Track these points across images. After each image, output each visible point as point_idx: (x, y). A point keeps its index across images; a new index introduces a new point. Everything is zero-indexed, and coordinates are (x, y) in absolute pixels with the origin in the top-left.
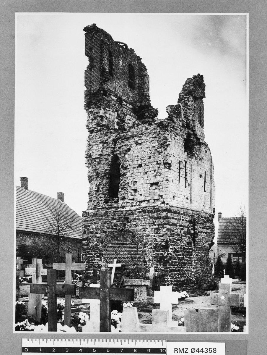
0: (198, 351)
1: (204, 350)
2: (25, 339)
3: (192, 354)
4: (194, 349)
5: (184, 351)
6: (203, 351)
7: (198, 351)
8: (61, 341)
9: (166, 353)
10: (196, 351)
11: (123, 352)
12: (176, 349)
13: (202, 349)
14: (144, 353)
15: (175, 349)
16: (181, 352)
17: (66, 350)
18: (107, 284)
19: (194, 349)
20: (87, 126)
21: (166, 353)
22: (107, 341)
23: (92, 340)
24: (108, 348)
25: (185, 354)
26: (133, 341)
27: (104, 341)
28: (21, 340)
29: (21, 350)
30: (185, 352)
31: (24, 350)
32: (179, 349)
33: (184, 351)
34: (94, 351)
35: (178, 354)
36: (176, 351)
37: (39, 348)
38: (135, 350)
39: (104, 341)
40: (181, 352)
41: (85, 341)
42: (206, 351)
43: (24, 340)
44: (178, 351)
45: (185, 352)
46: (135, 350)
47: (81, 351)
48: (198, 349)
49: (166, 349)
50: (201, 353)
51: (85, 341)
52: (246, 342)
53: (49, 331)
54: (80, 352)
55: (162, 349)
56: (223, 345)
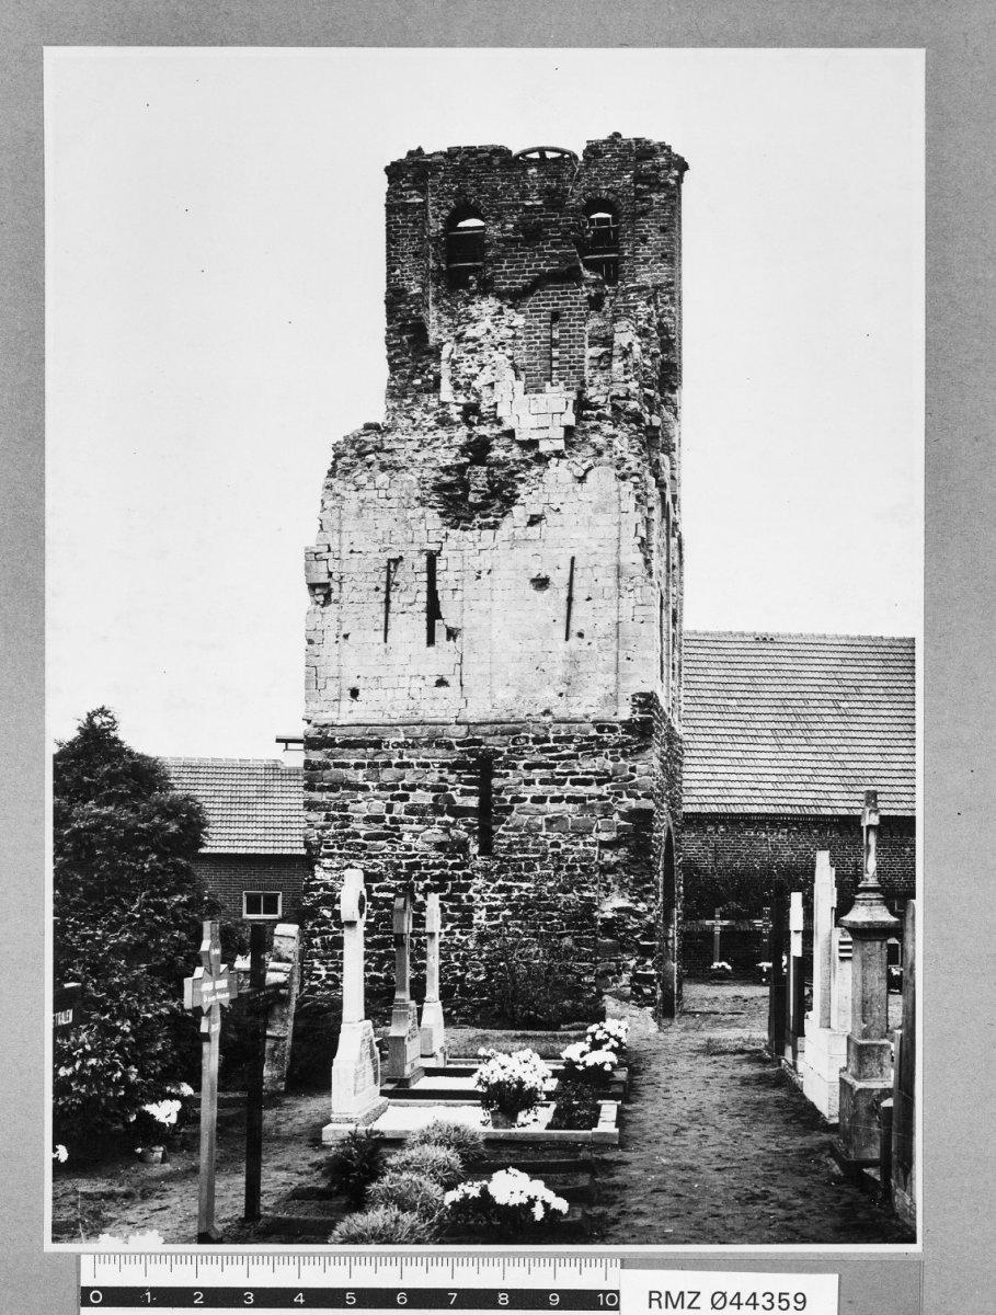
0: (736, 1301)
1: (761, 1300)
3: (715, 1312)
4: (724, 1295)
5: (686, 1304)
6: (755, 1305)
10: (731, 1304)
12: (655, 1296)
13: (754, 1294)
15: (651, 1292)
16: (675, 1307)
17: (246, 1298)
21: (617, 1308)
24: (554, 1291)
25: (686, 1311)
29: (75, 1295)
30: (689, 1307)
31: (86, 1296)
32: (668, 1293)
33: (686, 1304)
34: (351, 1300)
35: (664, 1311)
36: (655, 1303)
37: (143, 1290)
38: (503, 1299)
40: (675, 1307)
41: (317, 1262)
42: (769, 1305)
44: (663, 1300)
45: (689, 1307)
46: (503, 1299)
47: (302, 1301)
48: (738, 1294)
49: (617, 1292)
50: (746, 1310)
51: (317, 1262)
52: (920, 1264)
54: (298, 1306)
55: (605, 1292)
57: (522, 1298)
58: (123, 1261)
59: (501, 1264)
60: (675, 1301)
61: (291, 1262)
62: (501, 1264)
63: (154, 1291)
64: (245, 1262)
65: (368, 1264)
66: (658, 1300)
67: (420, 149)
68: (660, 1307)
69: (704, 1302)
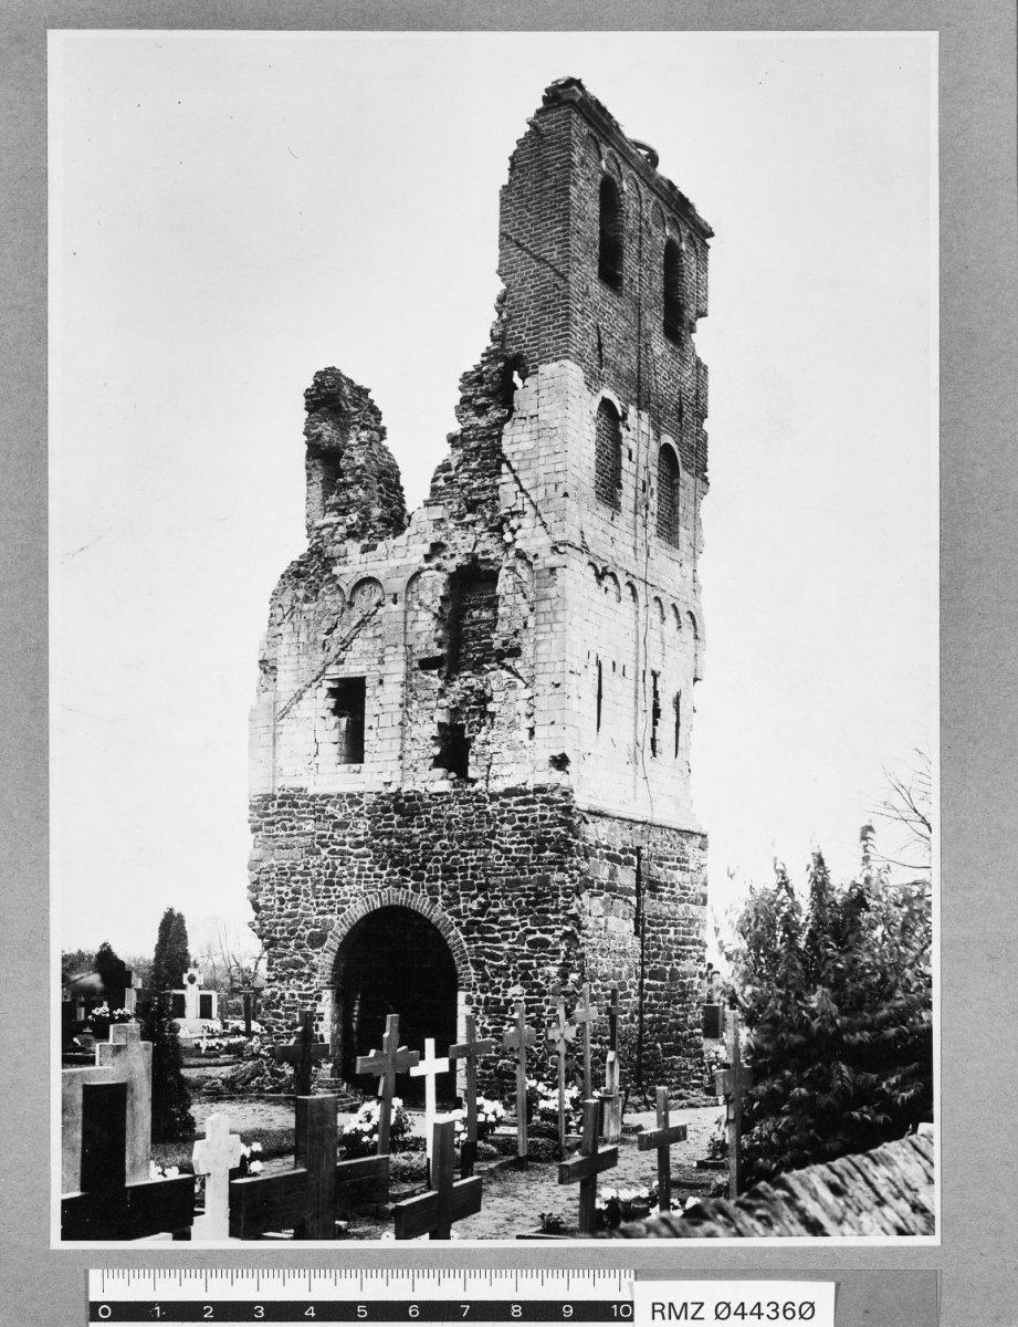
0: (740, 1311)
1: (766, 1310)
2: (100, 1271)
3: (719, 1323)
4: (728, 1305)
5: (690, 1315)
6: (759, 1314)
7: (743, 1314)
8: (467, 1276)
9: (631, 1319)
10: (735, 1314)
11: (471, 1317)
12: (658, 1307)
13: (759, 1304)
14: (226, 1321)
15: (654, 1304)
16: (678, 1318)
17: (256, 1312)
18: (195, 1076)
19: (728, 1305)
20: (261, 662)
21: (631, 1319)
22: (617, 1274)
23: (162, 1271)
25: (690, 1323)
26: (509, 1274)
27: (141, 1276)
28: (87, 1272)
29: (84, 1312)
30: (693, 1318)
31: (94, 1311)
32: (671, 1304)
33: (690, 1315)
34: (362, 1313)
35: (667, 1323)
36: (658, 1315)
38: (516, 1311)
39: (141, 1276)
40: (678, 1318)
41: (328, 1275)
42: (773, 1315)
43: (95, 1275)
44: (666, 1311)
45: (693, 1318)
46: (516, 1311)
47: (313, 1314)
48: (742, 1304)
49: (631, 1303)
50: (751, 1320)
51: (328, 1275)
52: (933, 1278)
53: (234, 1233)
54: (309, 1319)
55: (619, 1303)
56: (829, 1288)
57: (535, 1310)
58: (131, 1276)
59: (514, 1276)
60: (678, 1313)
61: (302, 1275)
62: (514, 1276)
63: (163, 1304)
64: (540, 1276)
65: (535, 1277)
66: (661, 1311)
67: (369, 391)
68: (664, 1318)
69: (708, 1312)
